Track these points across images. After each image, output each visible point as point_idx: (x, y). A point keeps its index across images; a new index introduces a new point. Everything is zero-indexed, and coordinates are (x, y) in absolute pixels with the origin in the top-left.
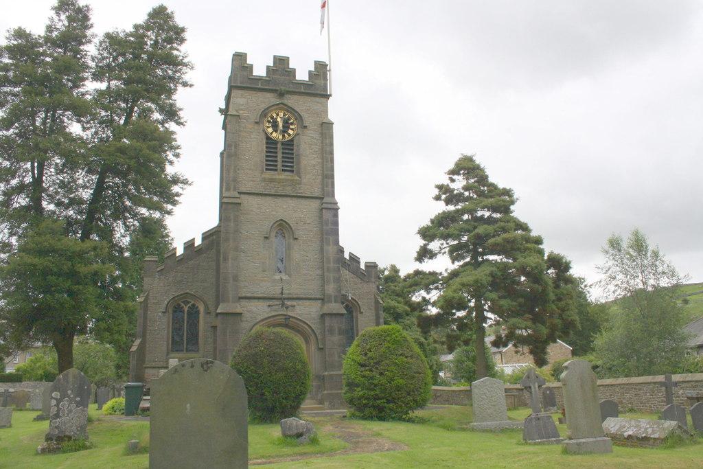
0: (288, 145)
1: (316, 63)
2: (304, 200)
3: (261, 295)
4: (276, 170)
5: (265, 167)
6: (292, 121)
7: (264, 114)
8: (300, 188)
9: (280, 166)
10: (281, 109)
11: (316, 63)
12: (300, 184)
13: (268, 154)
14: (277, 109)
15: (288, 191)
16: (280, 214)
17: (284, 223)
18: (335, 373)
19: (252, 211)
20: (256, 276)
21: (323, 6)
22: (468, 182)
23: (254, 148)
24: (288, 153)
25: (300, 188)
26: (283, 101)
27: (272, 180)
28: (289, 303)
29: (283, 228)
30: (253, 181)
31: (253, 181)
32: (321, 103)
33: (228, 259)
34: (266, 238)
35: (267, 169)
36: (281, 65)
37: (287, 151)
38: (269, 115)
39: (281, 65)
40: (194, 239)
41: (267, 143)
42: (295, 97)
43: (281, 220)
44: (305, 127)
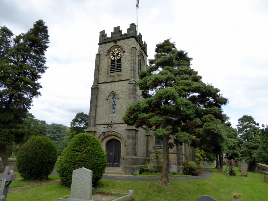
0: (119, 61)
1: (197, 72)
2: (122, 82)
3: (104, 123)
4: (114, 72)
5: (110, 72)
6: (120, 51)
7: (109, 51)
8: (121, 77)
9: (115, 70)
10: (116, 47)
11: (197, 72)
12: (121, 76)
13: (120, 65)
14: (114, 48)
15: (117, 79)
16: (113, 89)
17: (114, 93)
18: (129, 157)
19: (103, 90)
20: (103, 116)
21: (137, 6)
22: (31, 97)
23: (106, 64)
24: (119, 64)
25: (121, 77)
26: (116, 44)
27: (110, 76)
28: (113, 126)
29: (113, 94)
30: (104, 78)
31: (104, 78)
32: (131, 40)
33: (92, 110)
34: (107, 100)
35: (111, 73)
36: (117, 30)
37: (118, 64)
38: (121, 51)
39: (117, 30)
40: (192, 59)
41: (111, 62)
42: (121, 41)
43: (113, 92)
44: (124, 52)
